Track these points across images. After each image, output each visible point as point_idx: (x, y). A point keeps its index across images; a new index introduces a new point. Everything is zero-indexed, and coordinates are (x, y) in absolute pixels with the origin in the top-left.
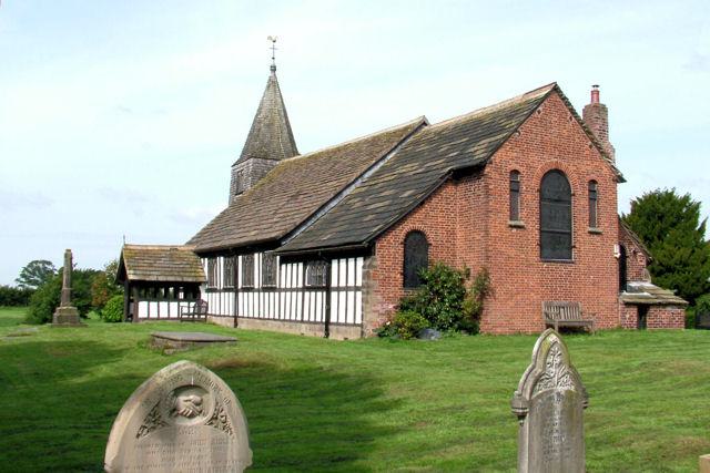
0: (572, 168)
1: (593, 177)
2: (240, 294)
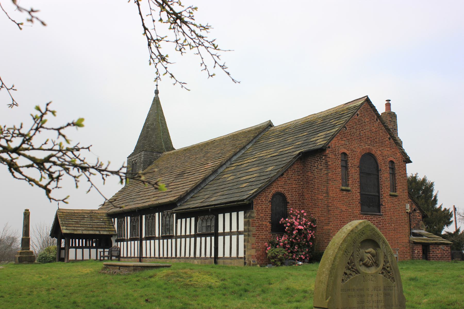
0: (379, 153)
1: (392, 159)
2: (144, 242)
